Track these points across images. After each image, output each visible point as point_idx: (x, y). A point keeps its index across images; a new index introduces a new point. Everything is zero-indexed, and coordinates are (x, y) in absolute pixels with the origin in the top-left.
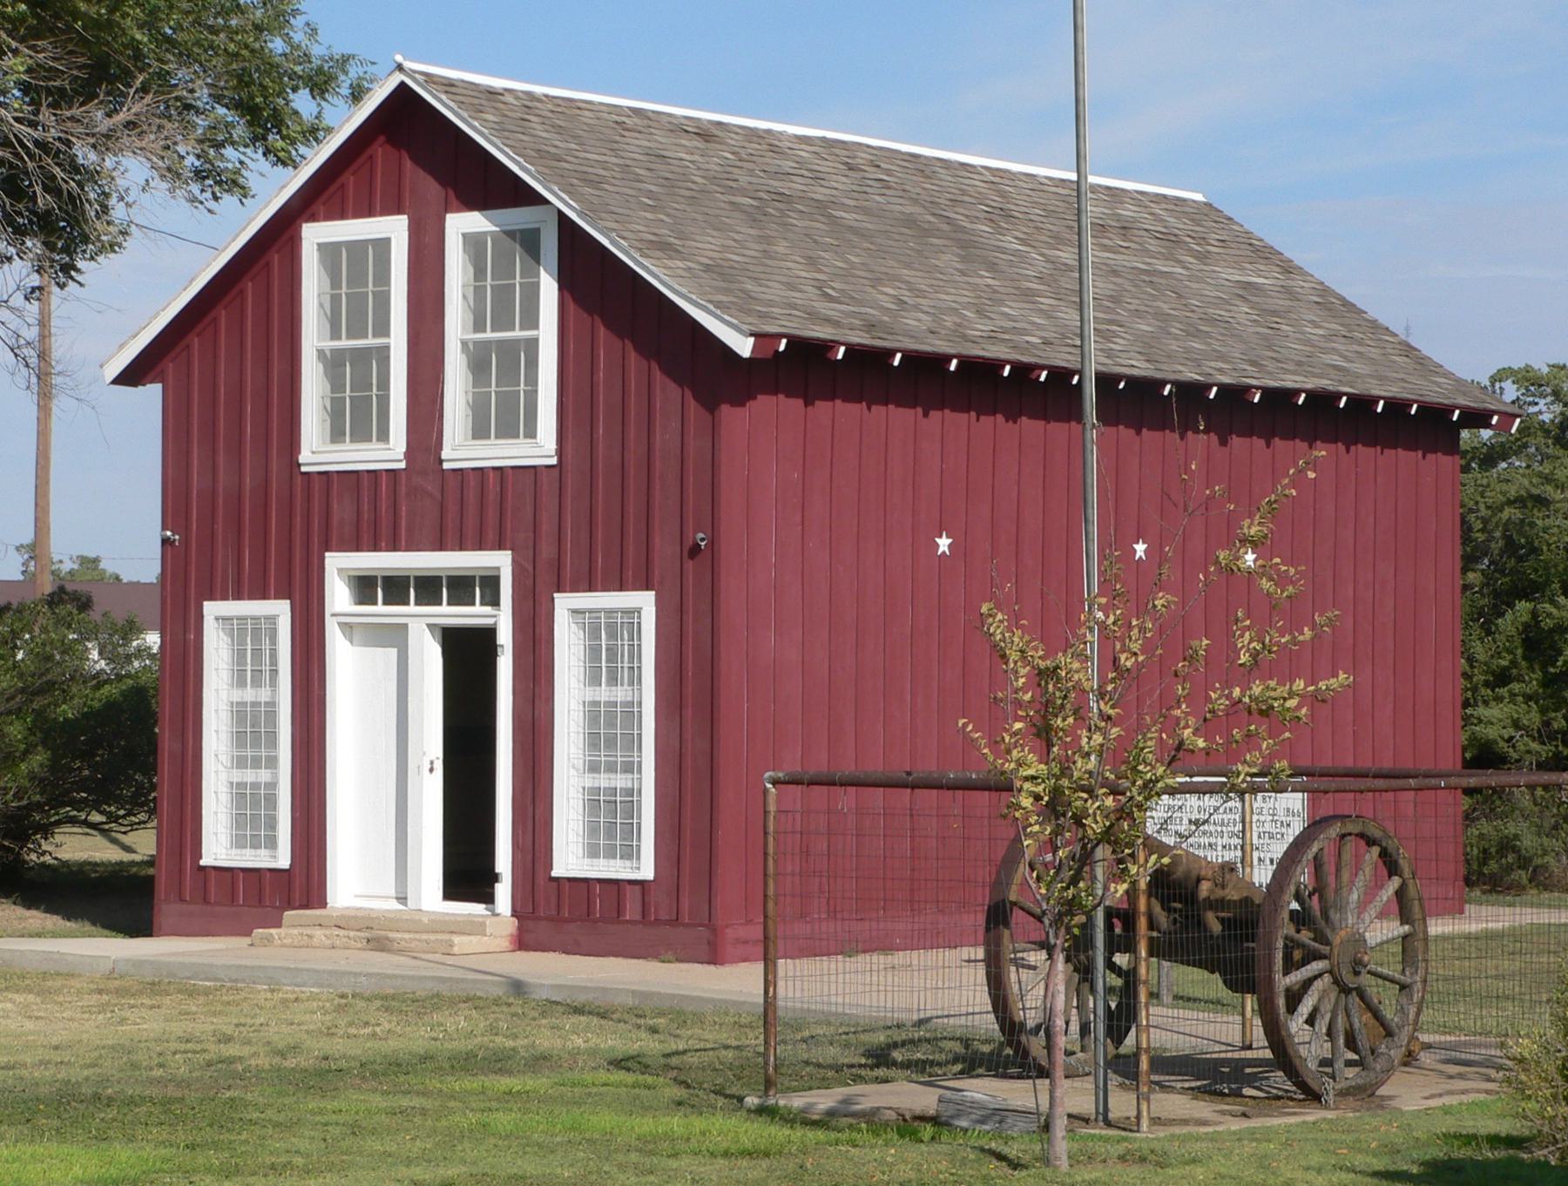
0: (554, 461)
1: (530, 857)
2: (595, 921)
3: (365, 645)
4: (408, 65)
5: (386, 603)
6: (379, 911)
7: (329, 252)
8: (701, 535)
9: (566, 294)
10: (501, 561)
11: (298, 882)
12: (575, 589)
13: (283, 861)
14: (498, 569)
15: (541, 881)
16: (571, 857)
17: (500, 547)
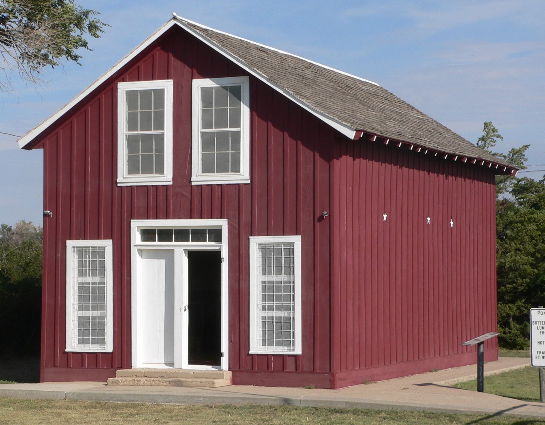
0: (249, 182)
1: (237, 346)
2: (272, 372)
3: (149, 259)
4: (178, 17)
5: (159, 241)
6: (159, 369)
7: (131, 95)
8: (325, 213)
9: (255, 114)
10: (223, 224)
11: (117, 358)
12: (260, 234)
13: (109, 348)
14: (221, 226)
15: (243, 355)
16: (257, 346)
17: (221, 217)
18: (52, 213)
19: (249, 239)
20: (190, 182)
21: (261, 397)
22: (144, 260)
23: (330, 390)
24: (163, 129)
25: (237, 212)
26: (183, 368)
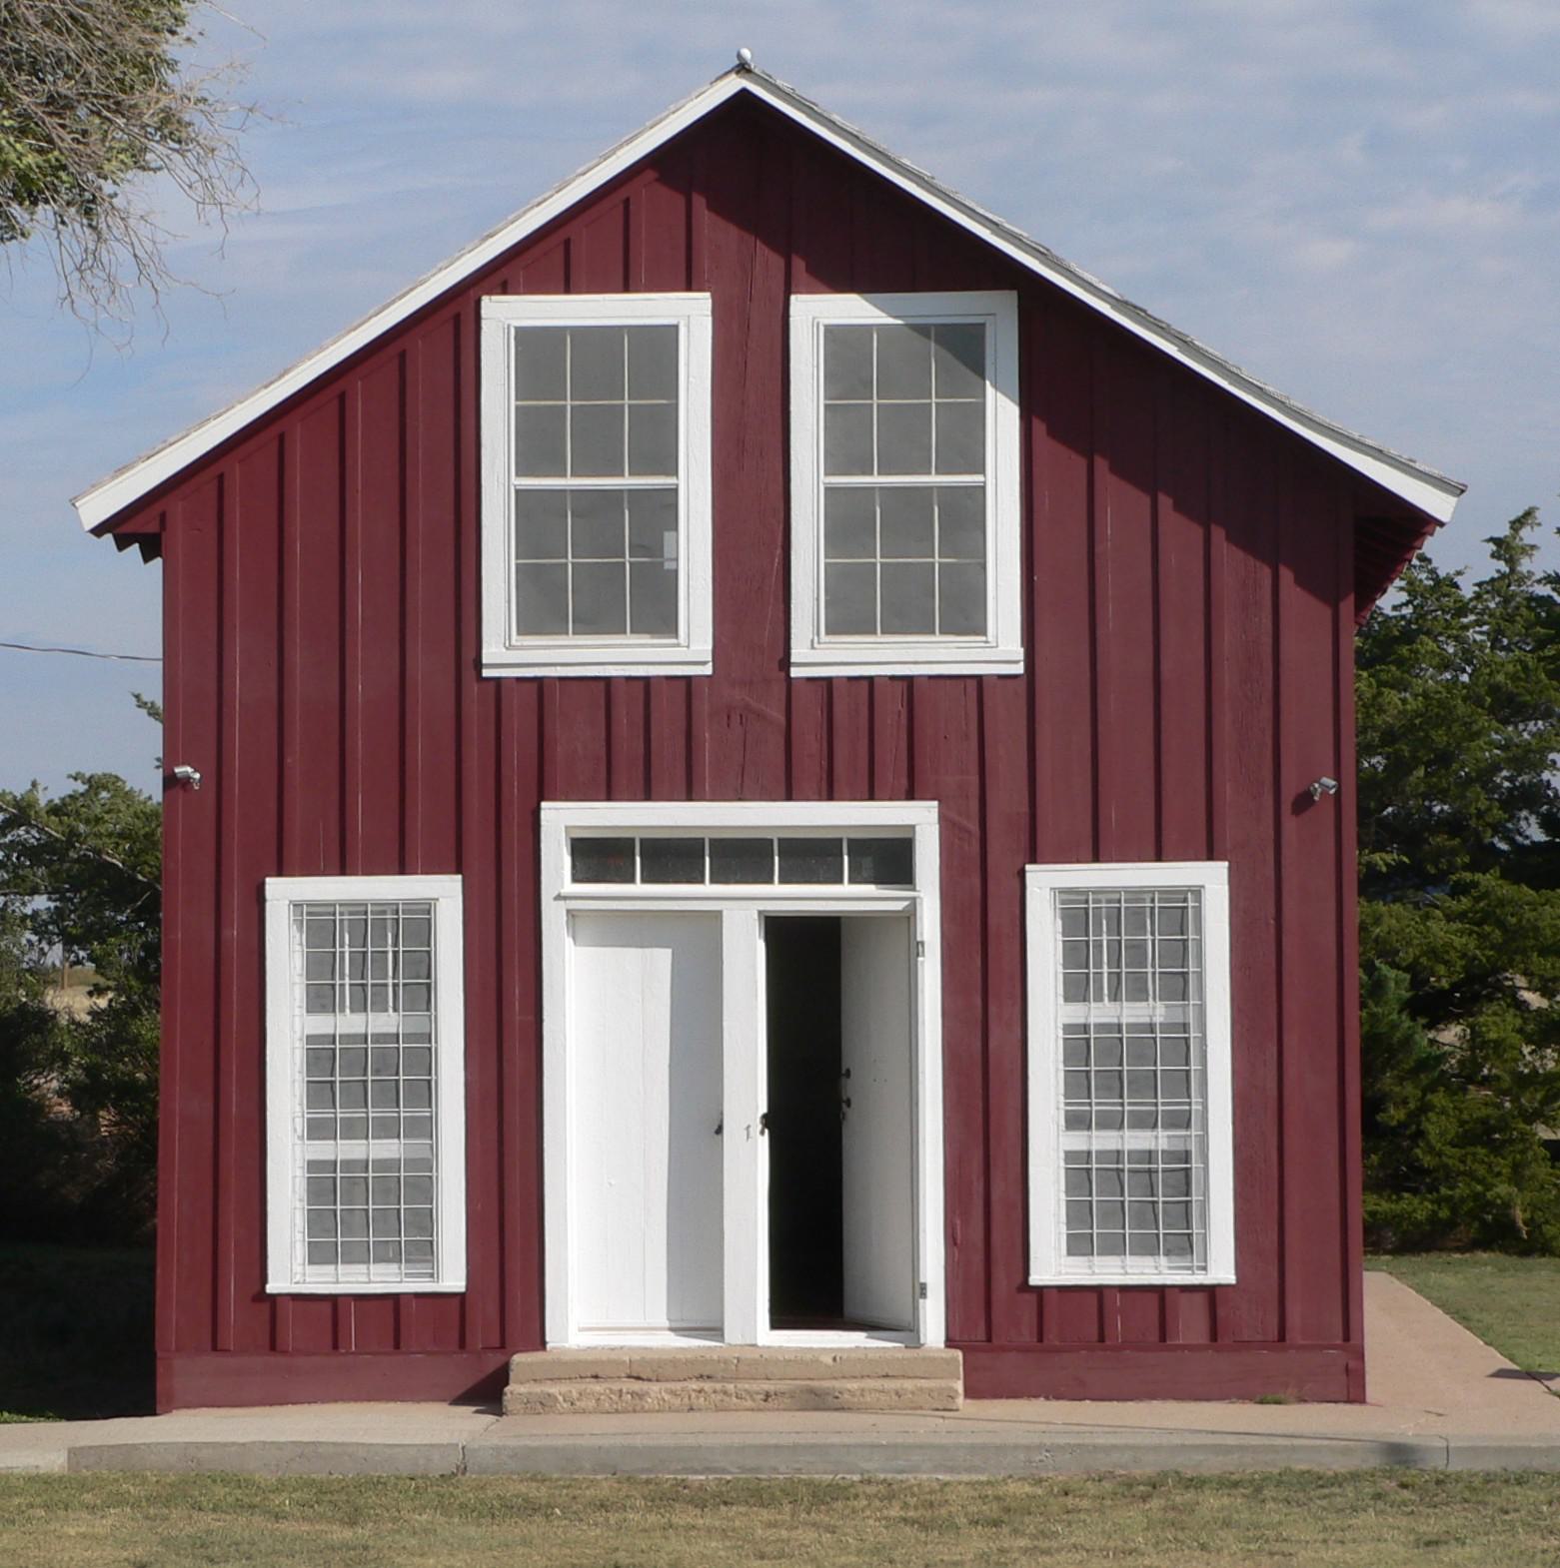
0: (1019, 669)
1: (978, 1258)
6: (631, 1349)
7: (533, 344)
9: (1039, 428)
11: (484, 1315)
12: (310, 868)
14: (913, 827)
18: (197, 776)
19: (1022, 874)
20: (786, 663)
21: (1266, 1441)
22: (578, 948)
23: (1348, 1407)
24: (675, 473)
25: (975, 779)
26: (760, 1344)
